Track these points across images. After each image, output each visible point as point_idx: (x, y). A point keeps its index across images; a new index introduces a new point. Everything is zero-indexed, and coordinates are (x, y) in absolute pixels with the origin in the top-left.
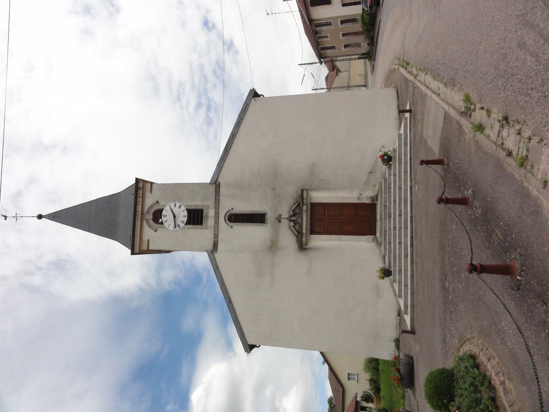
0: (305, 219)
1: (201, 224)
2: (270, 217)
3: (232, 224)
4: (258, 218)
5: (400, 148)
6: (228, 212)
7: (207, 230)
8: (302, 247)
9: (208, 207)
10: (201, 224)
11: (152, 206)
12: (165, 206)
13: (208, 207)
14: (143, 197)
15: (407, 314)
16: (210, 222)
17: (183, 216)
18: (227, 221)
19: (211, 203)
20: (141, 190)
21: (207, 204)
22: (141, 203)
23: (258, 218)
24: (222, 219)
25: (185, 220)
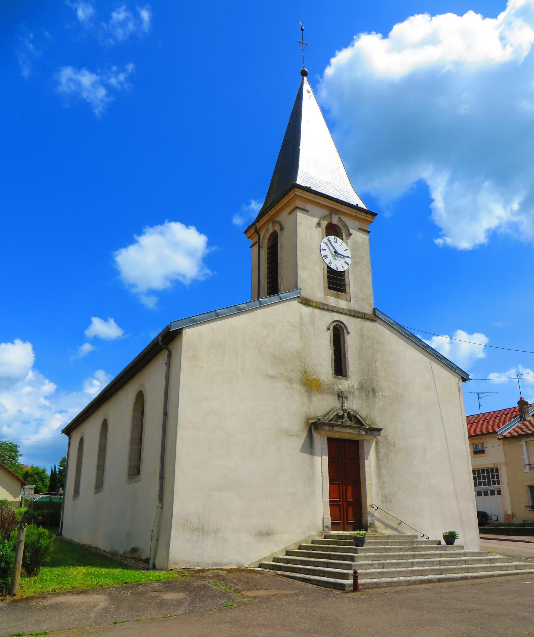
0: (348, 434)
1: (329, 288)
2: (344, 385)
3: (331, 328)
4: (340, 368)
5: (465, 554)
6: (346, 327)
7: (323, 294)
8: (314, 426)
9: (348, 300)
10: (329, 288)
11: (346, 226)
12: (347, 243)
13: (348, 300)
14: (356, 218)
15: (324, 538)
16: (332, 301)
17: (339, 265)
18: (335, 324)
19: (354, 305)
20: (355, 214)
21: (352, 299)
22: (350, 213)
23: (340, 368)
24: (343, 318)
25: (333, 267)
